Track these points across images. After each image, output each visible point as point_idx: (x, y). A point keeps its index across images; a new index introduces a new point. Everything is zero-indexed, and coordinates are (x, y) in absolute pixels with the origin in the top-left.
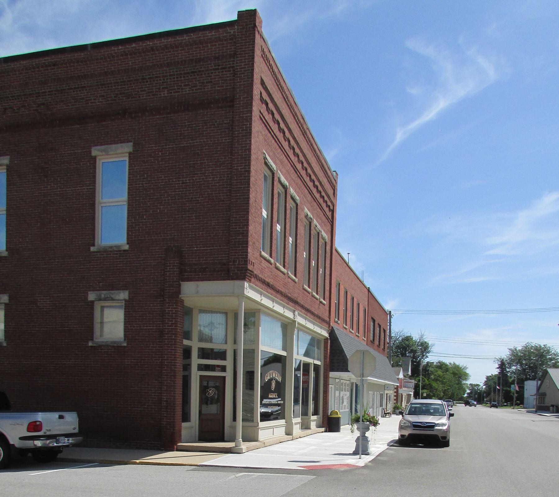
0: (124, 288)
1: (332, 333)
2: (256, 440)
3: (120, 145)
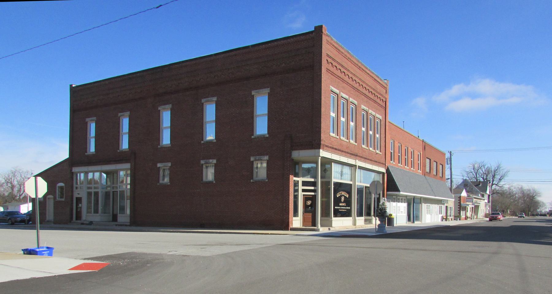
1: (388, 170)
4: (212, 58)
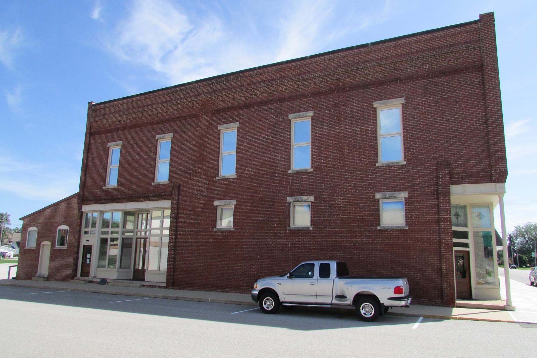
0: (404, 190)
2: (500, 300)
3: (394, 100)
4: (306, 62)
